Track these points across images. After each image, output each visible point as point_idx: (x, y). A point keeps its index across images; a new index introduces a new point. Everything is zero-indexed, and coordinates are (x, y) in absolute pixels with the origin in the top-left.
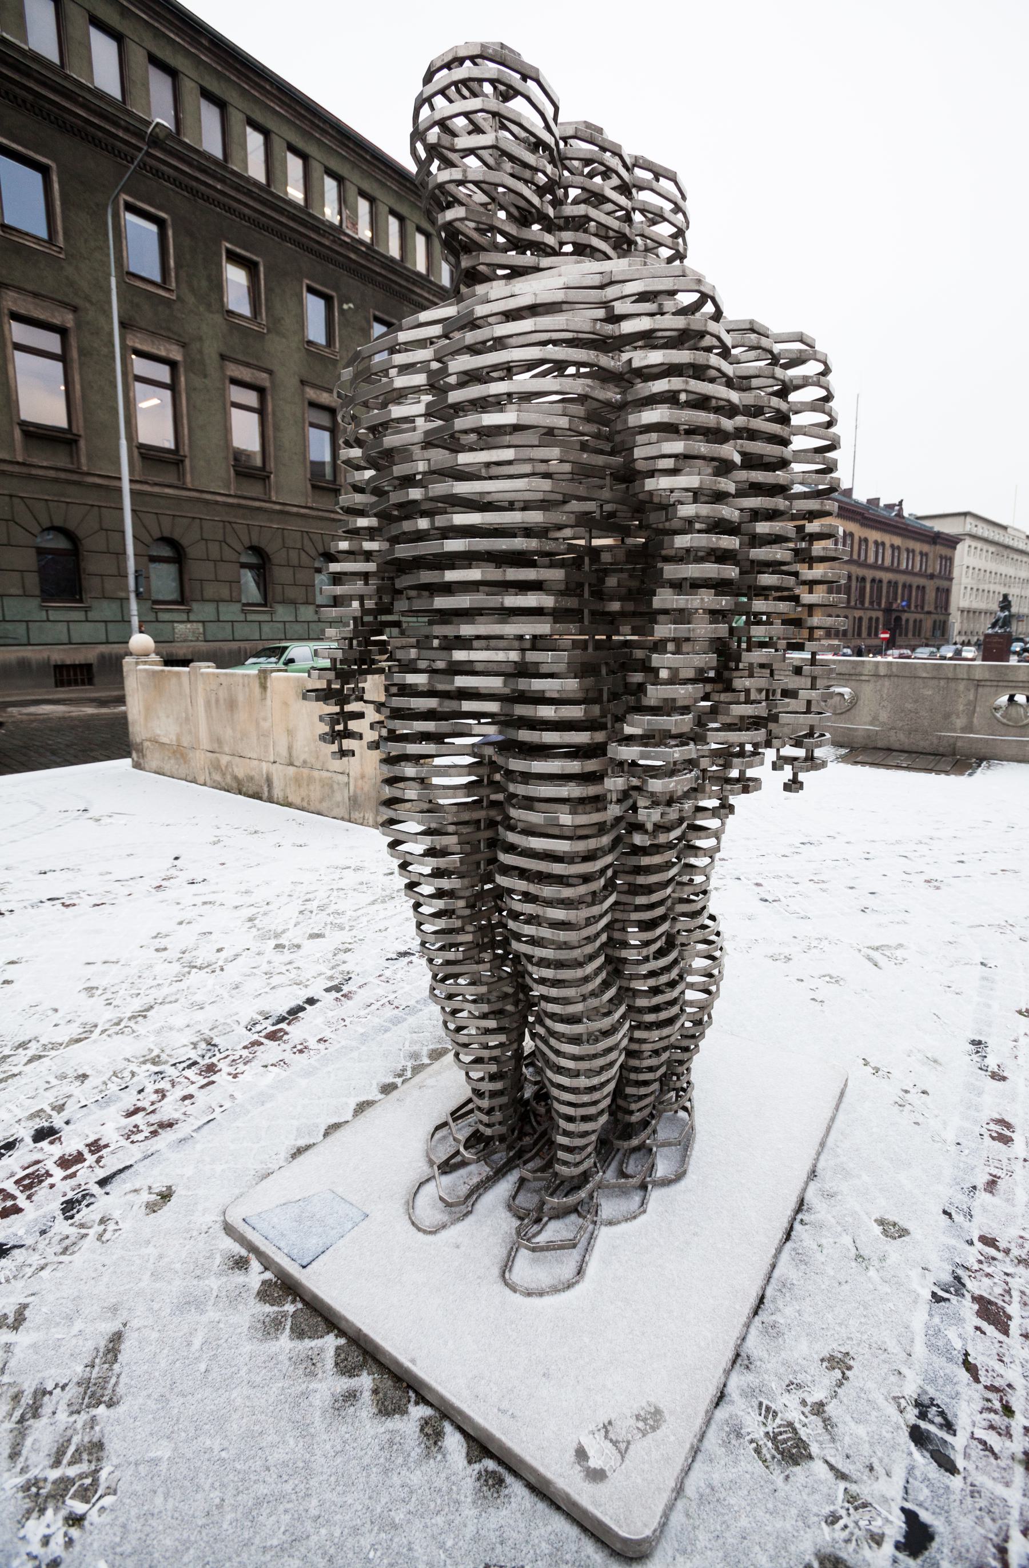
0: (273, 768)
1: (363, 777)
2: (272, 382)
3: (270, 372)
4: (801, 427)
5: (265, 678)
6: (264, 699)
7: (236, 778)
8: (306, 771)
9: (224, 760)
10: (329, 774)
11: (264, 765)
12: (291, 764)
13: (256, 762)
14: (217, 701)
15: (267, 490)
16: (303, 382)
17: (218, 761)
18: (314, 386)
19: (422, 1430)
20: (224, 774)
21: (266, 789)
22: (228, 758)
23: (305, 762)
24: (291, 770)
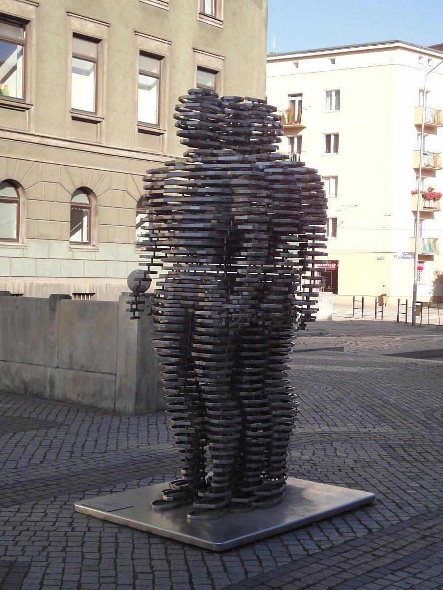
0: (56, 372)
1: (126, 376)
2: (39, 16)
3: (170, 43)
4: (317, 261)
5: (55, 303)
6: (52, 318)
7: (23, 381)
8: (82, 373)
9: (14, 367)
10: (101, 375)
11: (49, 370)
12: (72, 368)
13: (42, 368)
14: (13, 320)
15: (99, 134)
16: (68, 13)
17: (9, 367)
18: (147, 35)
19: (437, 200)
20: (13, 380)
21: (48, 389)
22: (19, 365)
23: (82, 366)
24: (71, 373)
